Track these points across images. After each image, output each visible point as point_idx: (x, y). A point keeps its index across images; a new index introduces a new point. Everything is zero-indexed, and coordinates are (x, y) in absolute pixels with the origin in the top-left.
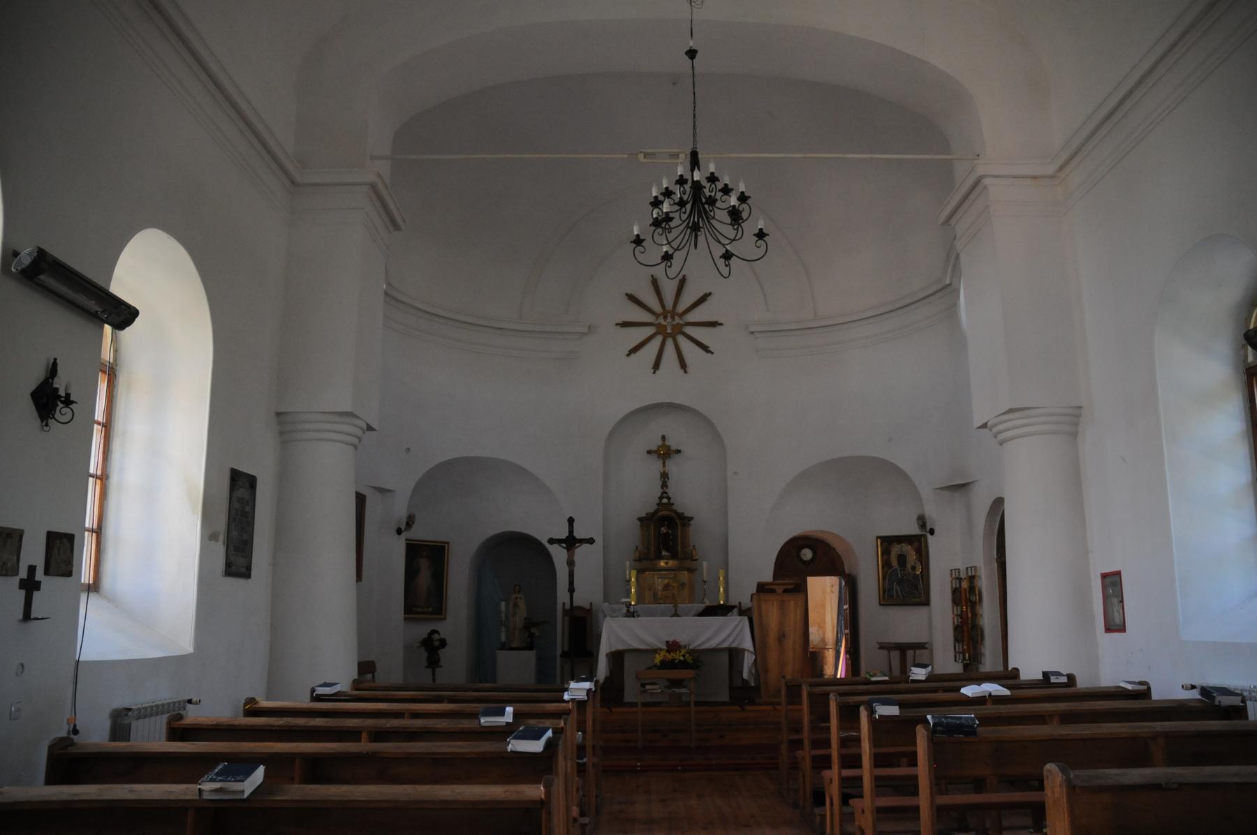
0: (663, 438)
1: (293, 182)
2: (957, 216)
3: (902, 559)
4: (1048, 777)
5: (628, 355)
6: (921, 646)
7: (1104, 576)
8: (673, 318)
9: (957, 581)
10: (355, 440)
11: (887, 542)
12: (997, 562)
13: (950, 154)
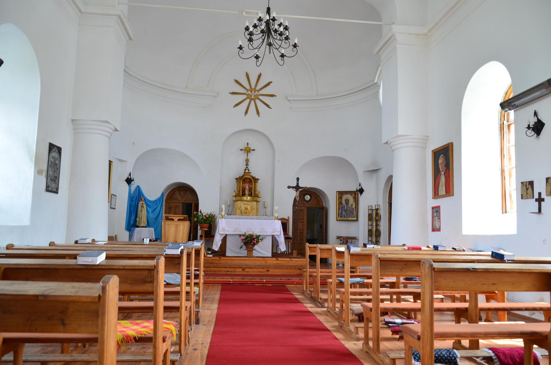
0: (248, 144)
1: (80, 11)
3: (347, 201)
4: (422, 265)
5: (234, 107)
6: (354, 238)
7: (433, 208)
9: (371, 210)
10: (109, 135)
11: (341, 194)
12: (388, 203)
13: (381, 21)
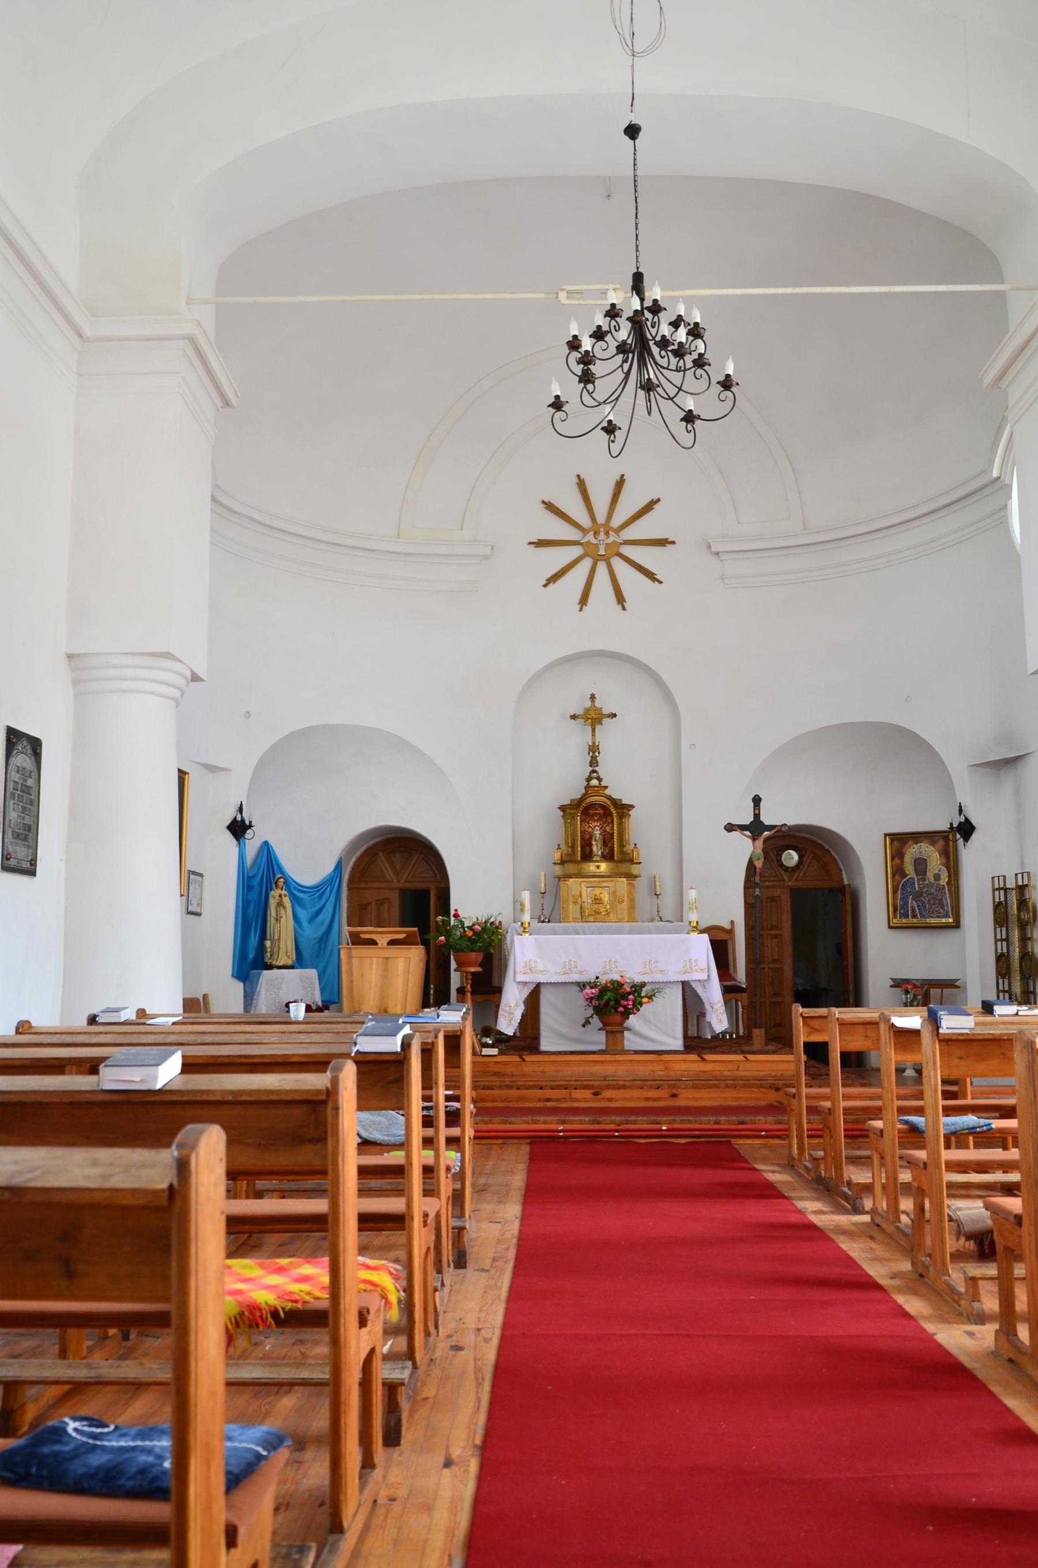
0: (593, 697)
2: (1008, 377)
3: (921, 864)
8: (607, 533)
10: (176, 693)
